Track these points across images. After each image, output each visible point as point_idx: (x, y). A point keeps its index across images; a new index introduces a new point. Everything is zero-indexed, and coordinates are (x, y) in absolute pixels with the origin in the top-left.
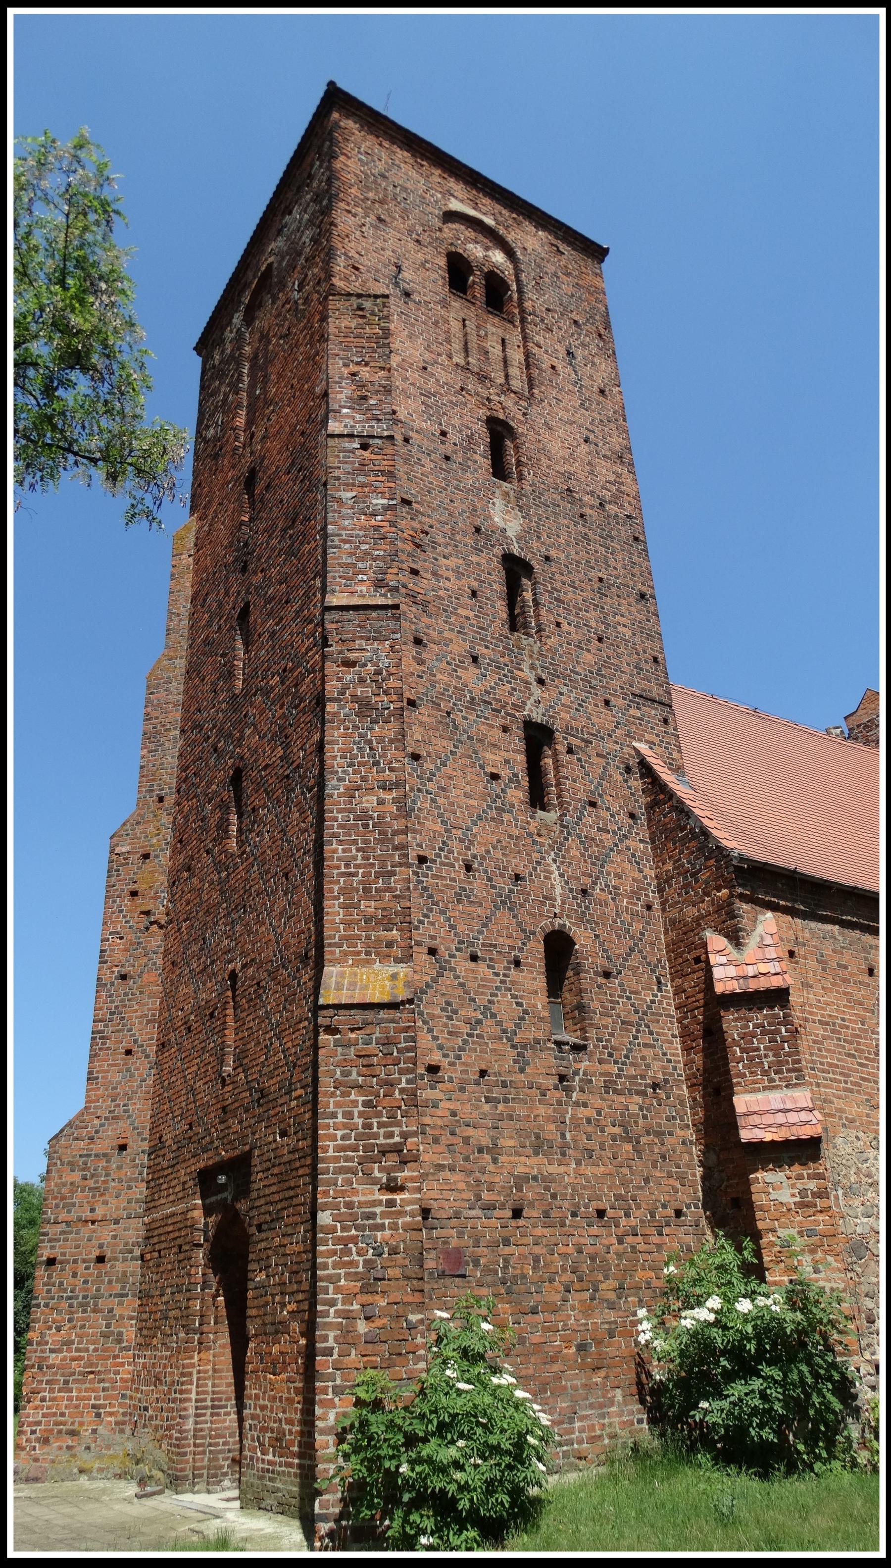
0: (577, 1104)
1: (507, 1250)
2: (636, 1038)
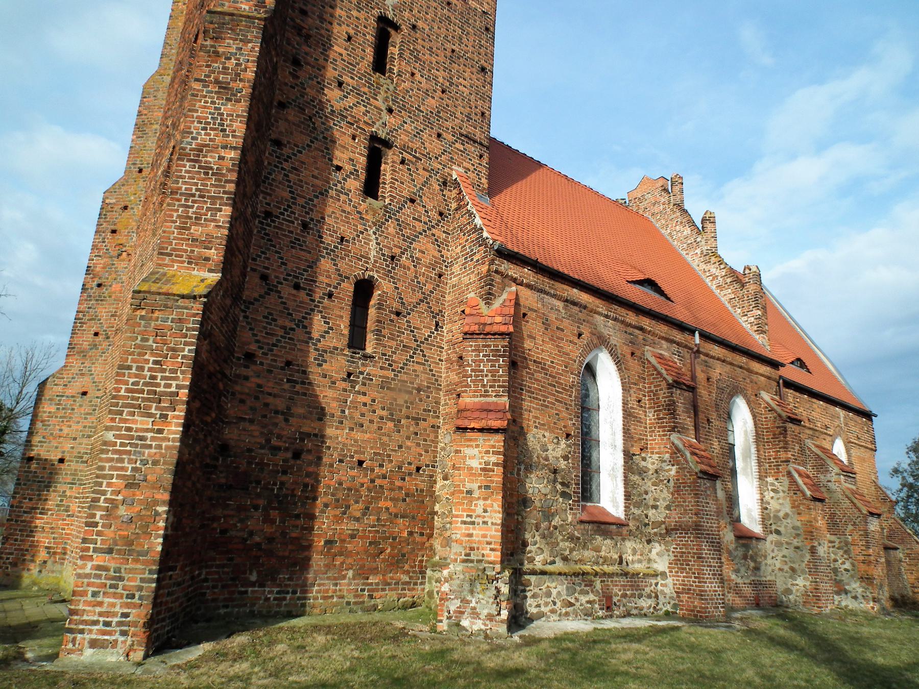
0: (359, 393)
1: (284, 478)
2: (412, 357)
